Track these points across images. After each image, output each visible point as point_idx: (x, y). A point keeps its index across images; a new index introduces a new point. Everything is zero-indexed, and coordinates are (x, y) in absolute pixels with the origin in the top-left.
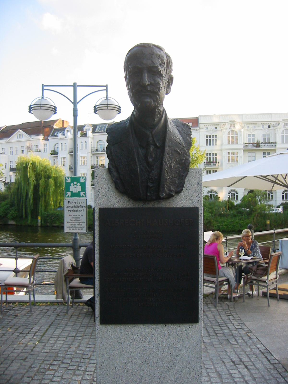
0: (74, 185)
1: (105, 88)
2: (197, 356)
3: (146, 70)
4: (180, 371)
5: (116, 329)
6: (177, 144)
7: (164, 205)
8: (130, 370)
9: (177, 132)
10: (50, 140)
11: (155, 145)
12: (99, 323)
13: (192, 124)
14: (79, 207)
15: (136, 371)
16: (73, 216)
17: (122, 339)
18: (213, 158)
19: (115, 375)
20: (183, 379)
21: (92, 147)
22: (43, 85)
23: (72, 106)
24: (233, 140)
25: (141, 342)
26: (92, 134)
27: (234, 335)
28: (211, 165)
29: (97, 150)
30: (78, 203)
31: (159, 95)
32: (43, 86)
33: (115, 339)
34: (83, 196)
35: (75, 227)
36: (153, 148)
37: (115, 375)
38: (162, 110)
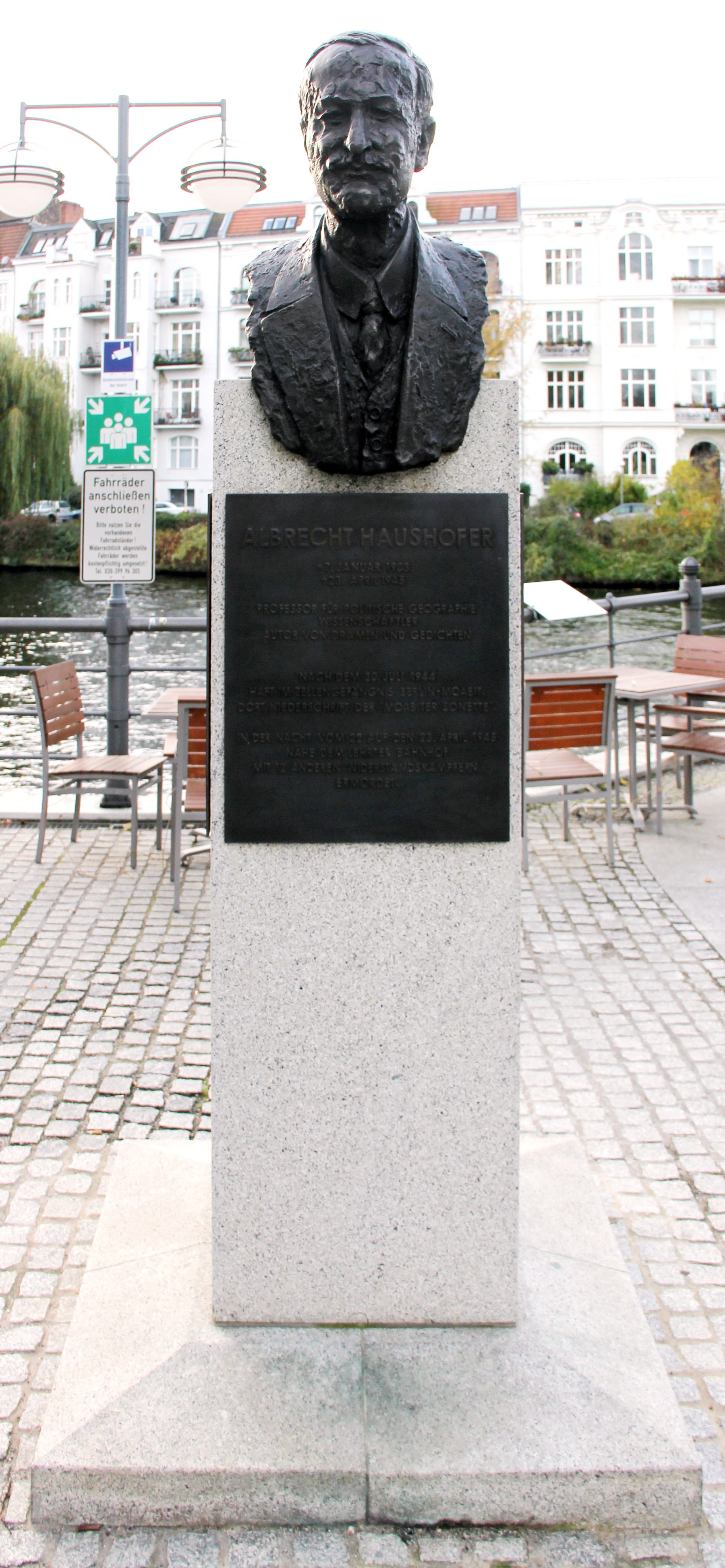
0: (115, 423)
1: (217, 110)
2: (505, 944)
3: (366, 111)
4: (454, 990)
5: (269, 856)
6: (447, 309)
7: (408, 485)
8: (310, 986)
9: (446, 276)
10: (17, 269)
11: (384, 313)
12: (222, 839)
13: (498, 210)
14: (128, 496)
15: (326, 987)
16: (112, 525)
17: (289, 890)
18: (570, 328)
19: (266, 999)
20: (464, 1016)
21: (159, 289)
22: (23, 104)
23: (115, 167)
24: (633, 262)
25: (341, 897)
26: (157, 245)
27: (631, 929)
28: (561, 350)
29: (175, 301)
30: (125, 484)
31: (396, 177)
32: (25, 108)
33: (267, 887)
34: (142, 461)
35: (114, 563)
36: (377, 321)
37: (266, 999)
38: (403, 215)
